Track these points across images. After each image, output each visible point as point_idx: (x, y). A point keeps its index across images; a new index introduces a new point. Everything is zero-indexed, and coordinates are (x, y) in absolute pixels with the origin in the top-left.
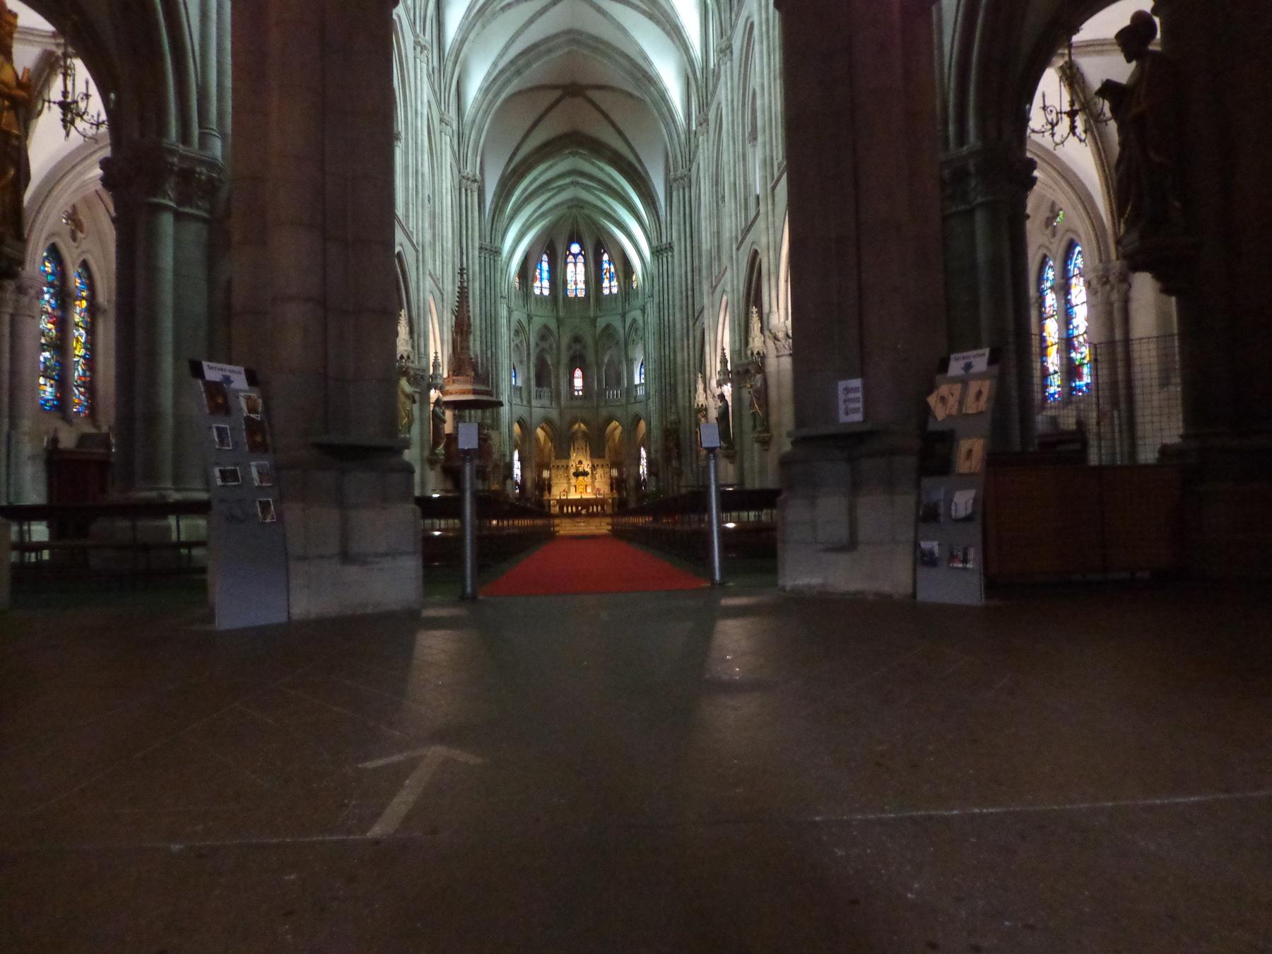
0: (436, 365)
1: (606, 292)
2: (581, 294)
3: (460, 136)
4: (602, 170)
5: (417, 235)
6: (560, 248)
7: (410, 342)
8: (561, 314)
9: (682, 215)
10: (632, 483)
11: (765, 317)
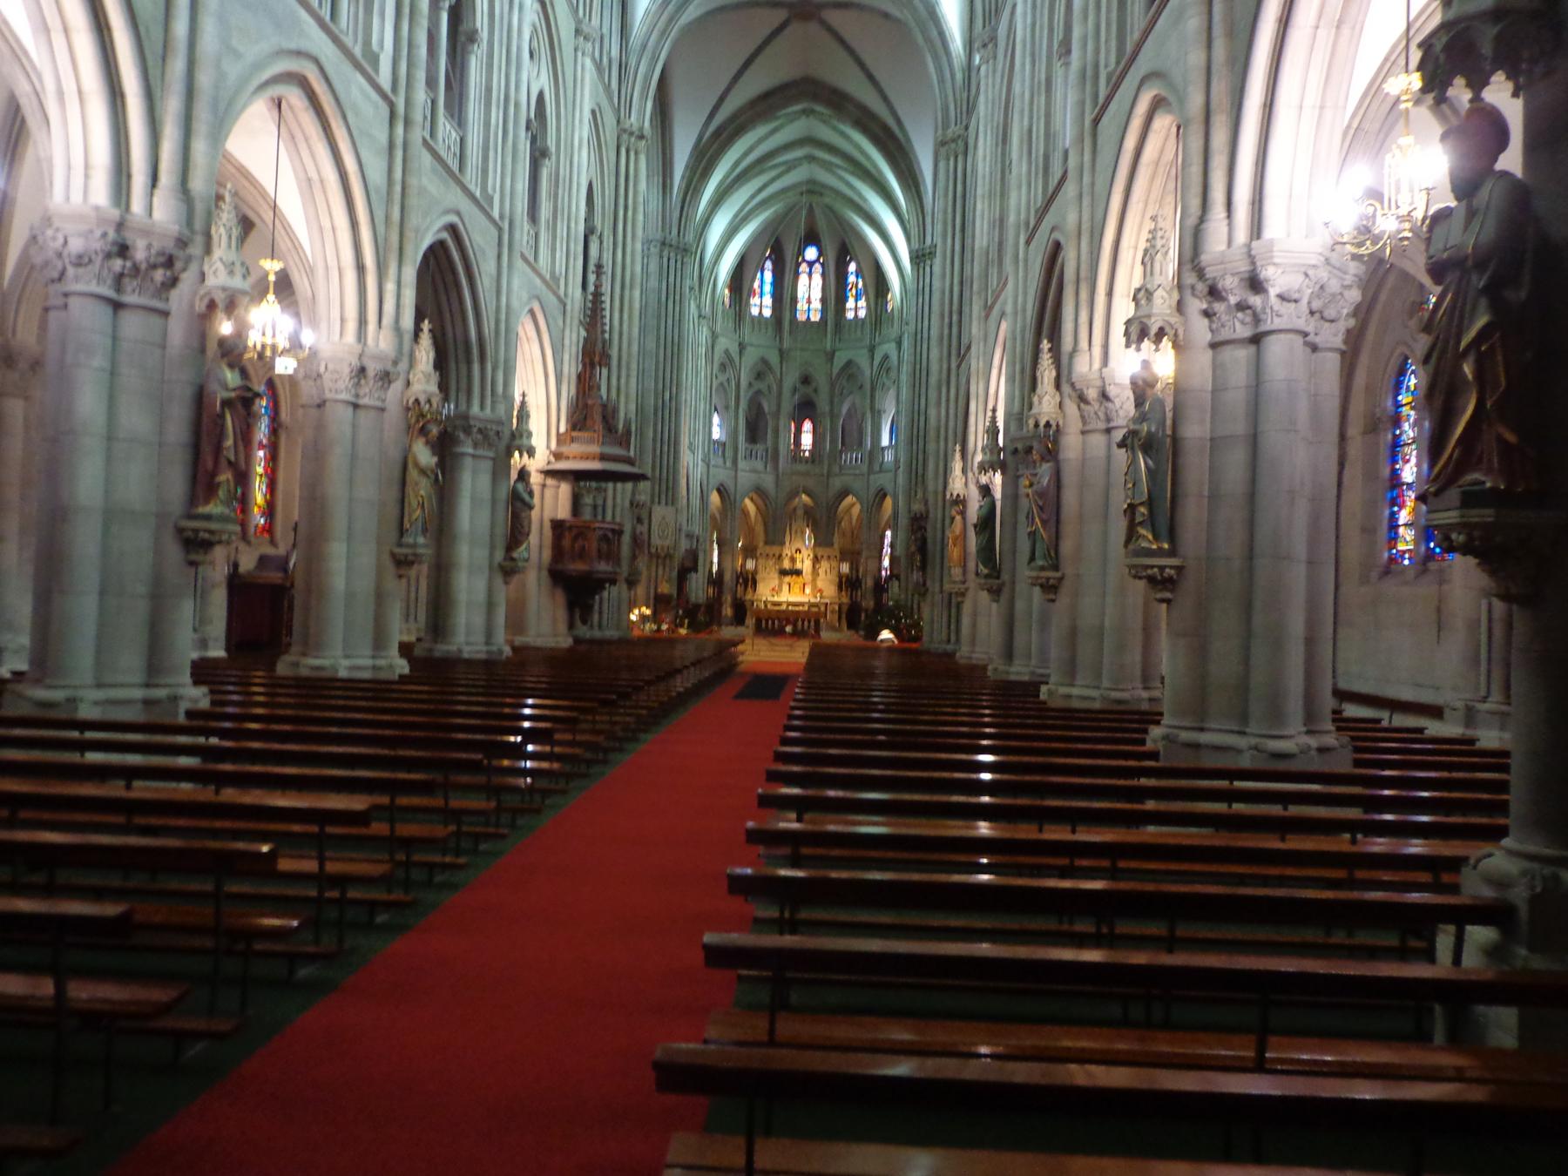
1: (850, 315)
6: (789, 250)
10: (870, 582)
11: (1065, 360)
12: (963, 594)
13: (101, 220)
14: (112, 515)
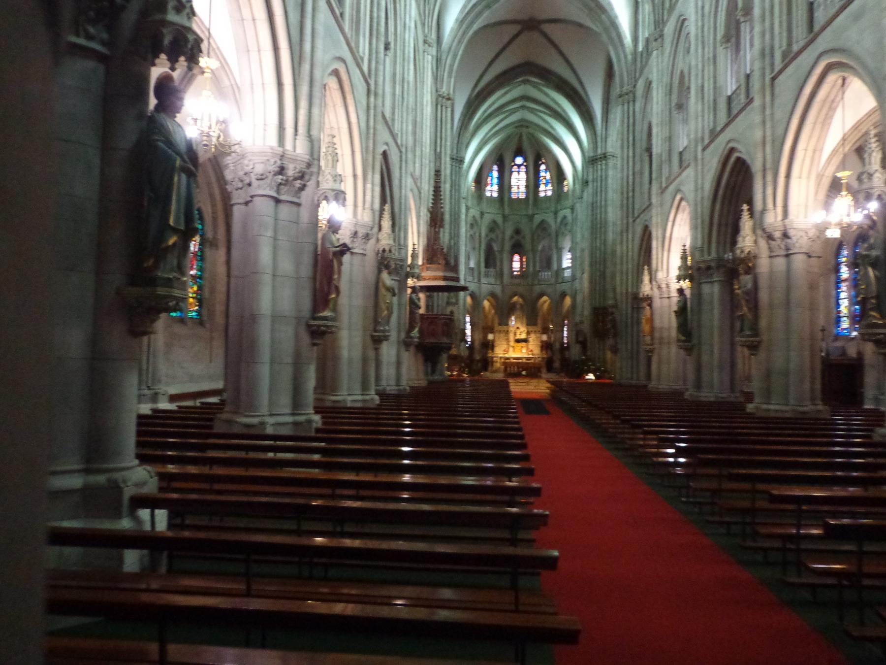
0: (414, 256)
1: (542, 194)
2: (522, 196)
3: (438, 60)
4: (546, 94)
5: (402, 137)
6: (507, 161)
7: (392, 236)
8: (507, 211)
9: (626, 125)
10: (557, 345)
12: (651, 351)
13: (274, 154)
14: (275, 318)
